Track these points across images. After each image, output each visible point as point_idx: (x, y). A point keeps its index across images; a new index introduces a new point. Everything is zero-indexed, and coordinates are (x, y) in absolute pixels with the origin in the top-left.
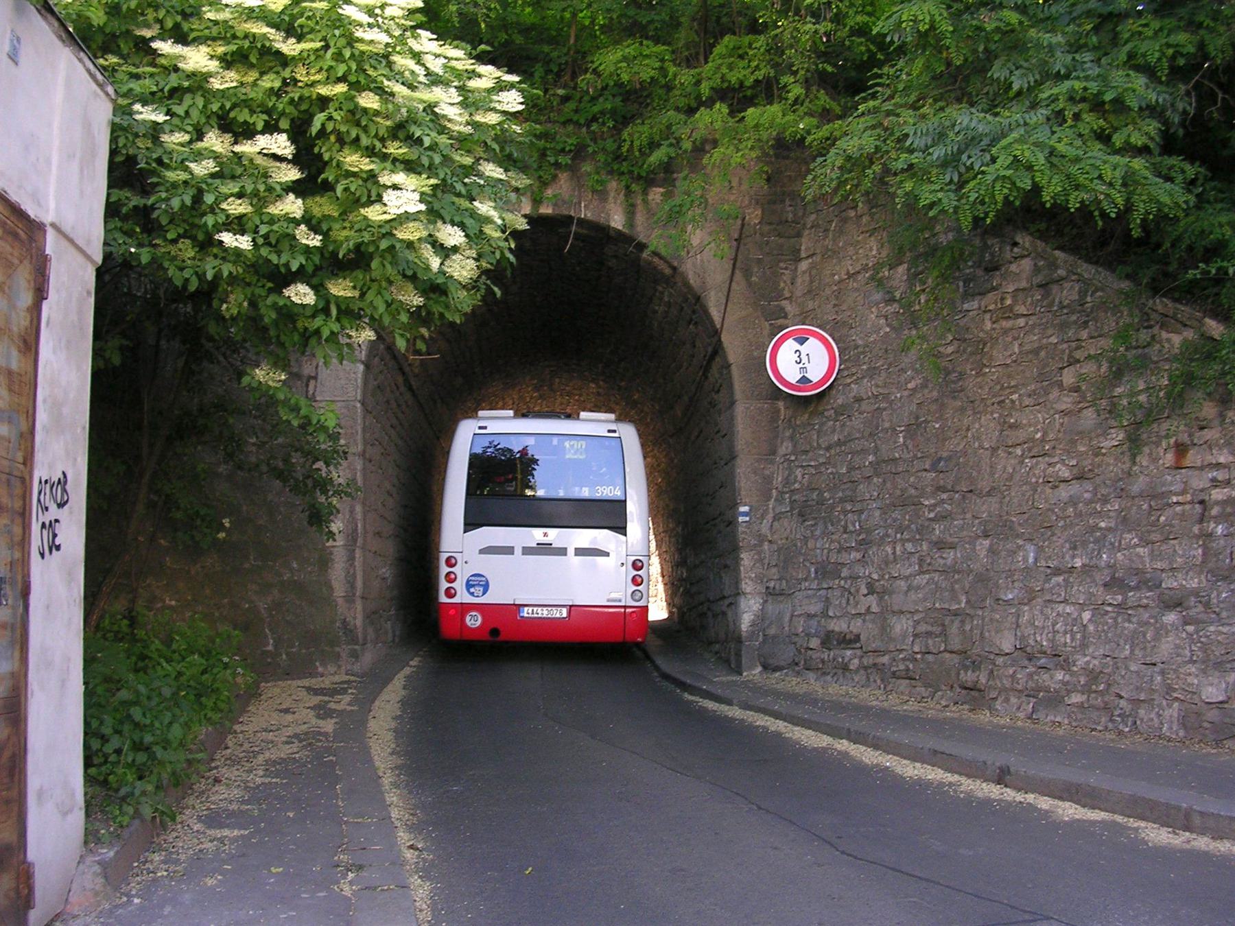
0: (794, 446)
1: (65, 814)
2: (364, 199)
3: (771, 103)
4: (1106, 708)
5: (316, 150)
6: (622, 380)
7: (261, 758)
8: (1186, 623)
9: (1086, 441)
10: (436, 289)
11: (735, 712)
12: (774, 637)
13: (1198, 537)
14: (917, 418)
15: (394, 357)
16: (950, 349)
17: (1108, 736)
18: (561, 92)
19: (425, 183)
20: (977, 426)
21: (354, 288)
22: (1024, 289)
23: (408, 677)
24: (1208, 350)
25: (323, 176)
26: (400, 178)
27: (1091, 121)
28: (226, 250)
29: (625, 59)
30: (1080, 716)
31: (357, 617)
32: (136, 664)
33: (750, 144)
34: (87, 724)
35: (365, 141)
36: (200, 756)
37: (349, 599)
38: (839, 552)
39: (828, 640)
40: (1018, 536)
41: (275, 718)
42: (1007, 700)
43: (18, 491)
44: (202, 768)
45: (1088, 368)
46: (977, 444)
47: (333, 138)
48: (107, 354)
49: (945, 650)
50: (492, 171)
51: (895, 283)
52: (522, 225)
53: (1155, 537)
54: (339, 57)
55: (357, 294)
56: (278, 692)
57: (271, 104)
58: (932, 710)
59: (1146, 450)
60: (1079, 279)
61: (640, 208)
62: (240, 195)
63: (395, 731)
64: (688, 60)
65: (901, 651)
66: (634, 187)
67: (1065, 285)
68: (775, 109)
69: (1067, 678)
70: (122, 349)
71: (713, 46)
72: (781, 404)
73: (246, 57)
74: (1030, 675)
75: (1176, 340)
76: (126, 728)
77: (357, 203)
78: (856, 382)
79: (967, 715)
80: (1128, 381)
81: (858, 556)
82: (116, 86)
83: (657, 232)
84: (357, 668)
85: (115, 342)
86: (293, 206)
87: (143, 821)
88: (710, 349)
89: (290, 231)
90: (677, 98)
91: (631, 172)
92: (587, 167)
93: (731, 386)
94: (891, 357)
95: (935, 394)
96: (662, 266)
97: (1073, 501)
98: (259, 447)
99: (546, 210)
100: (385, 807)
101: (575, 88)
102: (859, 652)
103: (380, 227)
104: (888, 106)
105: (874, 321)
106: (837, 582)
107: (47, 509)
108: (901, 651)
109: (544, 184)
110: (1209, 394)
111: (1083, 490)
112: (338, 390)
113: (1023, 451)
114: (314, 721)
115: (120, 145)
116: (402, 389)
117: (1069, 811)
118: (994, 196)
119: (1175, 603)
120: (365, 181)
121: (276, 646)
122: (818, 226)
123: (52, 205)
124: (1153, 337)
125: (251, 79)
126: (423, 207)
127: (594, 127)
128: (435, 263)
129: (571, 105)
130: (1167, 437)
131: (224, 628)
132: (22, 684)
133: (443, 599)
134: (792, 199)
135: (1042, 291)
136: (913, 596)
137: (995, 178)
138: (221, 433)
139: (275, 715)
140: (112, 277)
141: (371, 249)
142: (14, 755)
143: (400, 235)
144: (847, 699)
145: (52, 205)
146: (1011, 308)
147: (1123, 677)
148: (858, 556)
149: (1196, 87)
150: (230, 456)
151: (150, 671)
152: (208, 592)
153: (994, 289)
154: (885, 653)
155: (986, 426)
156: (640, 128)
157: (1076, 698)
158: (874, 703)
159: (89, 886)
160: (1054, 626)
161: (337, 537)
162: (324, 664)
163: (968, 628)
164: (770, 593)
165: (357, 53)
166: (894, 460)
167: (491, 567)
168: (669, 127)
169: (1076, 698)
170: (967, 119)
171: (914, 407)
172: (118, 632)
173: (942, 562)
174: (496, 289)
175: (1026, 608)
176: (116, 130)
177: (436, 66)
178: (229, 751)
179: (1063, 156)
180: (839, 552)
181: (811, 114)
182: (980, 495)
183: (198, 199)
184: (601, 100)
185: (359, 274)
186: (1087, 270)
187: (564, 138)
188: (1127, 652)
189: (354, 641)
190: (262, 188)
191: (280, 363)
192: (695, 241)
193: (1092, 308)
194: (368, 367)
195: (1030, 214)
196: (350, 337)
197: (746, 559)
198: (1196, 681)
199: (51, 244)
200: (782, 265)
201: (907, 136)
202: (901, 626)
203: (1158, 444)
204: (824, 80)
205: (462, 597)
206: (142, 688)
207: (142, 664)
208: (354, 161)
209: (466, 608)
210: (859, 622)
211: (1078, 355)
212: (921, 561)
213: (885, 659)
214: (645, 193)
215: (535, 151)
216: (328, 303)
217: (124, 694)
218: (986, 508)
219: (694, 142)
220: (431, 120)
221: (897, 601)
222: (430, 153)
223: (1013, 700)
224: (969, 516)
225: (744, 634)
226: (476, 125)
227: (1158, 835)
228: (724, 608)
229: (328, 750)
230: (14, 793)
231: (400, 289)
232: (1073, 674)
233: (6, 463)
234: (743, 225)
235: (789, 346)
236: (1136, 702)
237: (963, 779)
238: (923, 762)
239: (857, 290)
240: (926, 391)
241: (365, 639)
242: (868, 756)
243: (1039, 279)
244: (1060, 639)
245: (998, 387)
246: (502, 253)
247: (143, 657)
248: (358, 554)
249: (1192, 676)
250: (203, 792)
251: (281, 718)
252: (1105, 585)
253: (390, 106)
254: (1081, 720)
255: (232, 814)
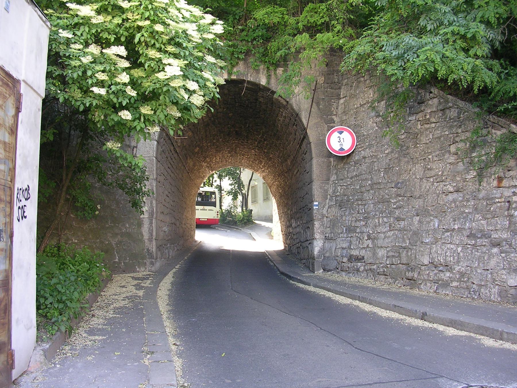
0: (337, 177)
1: (28, 329)
2: (157, 70)
3: (328, 32)
4: (467, 288)
5: (136, 49)
6: (265, 149)
7: (112, 306)
8: (501, 253)
9: (460, 176)
10: (186, 108)
11: (311, 289)
12: (328, 257)
13: (507, 216)
14: (389, 165)
15: (170, 139)
16: (403, 137)
17: (468, 300)
18: (240, 27)
19: (182, 63)
20: (414, 169)
21: (152, 110)
22: (435, 112)
23: (174, 273)
24: (513, 137)
25: (139, 60)
26: (171, 61)
27: (460, 43)
28: (95, 94)
29: (267, 13)
30: (456, 291)
31: (153, 247)
32: (60, 266)
33: (318, 49)
34: (38, 291)
35: (157, 45)
36: (86, 305)
37: (150, 240)
38: (355, 222)
39: (351, 258)
40: (431, 215)
41: (118, 290)
42: (426, 284)
43: (8, 193)
44: (87, 310)
45: (461, 145)
46: (414, 177)
47: (143, 44)
48: (47, 136)
49: (400, 263)
50: (210, 59)
51: (381, 109)
52: (223, 82)
53: (488, 216)
54: (146, 8)
55: (153, 112)
56: (119, 279)
57: (117, 31)
58: (394, 288)
59: (485, 180)
60: (458, 107)
61: (273, 76)
62: (103, 71)
63: (169, 295)
64: (293, 14)
65: (381, 263)
66: (271, 68)
67: (452, 110)
68: (330, 34)
69: (451, 275)
70: (54, 134)
71: (304, 8)
72: (332, 159)
73: (106, 10)
74: (436, 274)
75: (498, 133)
76: (55, 294)
77: (154, 71)
78: (363, 150)
79: (409, 290)
80: (478, 151)
81: (364, 223)
82: (51, 23)
83: (280, 87)
84: (153, 269)
85: (50, 132)
86: (124, 78)
87: (61, 332)
88: (302, 137)
89: (123, 89)
90: (289, 30)
91: (269, 61)
92: (251, 60)
93: (311, 152)
94: (378, 140)
95: (397, 155)
96: (282, 101)
97: (454, 201)
98: (112, 175)
99: (234, 77)
100: (164, 327)
101: (246, 26)
102: (364, 264)
103: (163, 81)
104: (376, 34)
105: (371, 125)
106: (355, 234)
107: (21, 201)
108: (381, 263)
109: (233, 66)
110: (512, 157)
111: (458, 196)
112: (146, 151)
113: (433, 179)
114: (135, 291)
115: (53, 47)
116: (173, 152)
117: (451, 331)
118: (418, 73)
119: (497, 244)
120: (157, 62)
121: (119, 260)
122: (348, 84)
123: (23, 72)
124: (489, 132)
125: (108, 20)
126: (182, 73)
127: (255, 42)
128: (186, 96)
129: (245, 33)
130: (494, 174)
131: (97, 252)
132: (10, 274)
134: (337, 73)
135: (442, 112)
136: (387, 240)
137: (417, 65)
138: (96, 169)
139: (118, 288)
140: (49, 103)
141: (160, 91)
142: (6, 304)
143: (172, 84)
144: (358, 284)
145: (23, 72)
146: (429, 119)
147: (474, 275)
148: (364, 223)
149: (507, 27)
150: (100, 179)
151: (66, 270)
152: (91, 236)
153: (422, 111)
154: (374, 264)
155: (418, 169)
156: (273, 43)
157: (455, 284)
158: (370, 285)
159: (38, 359)
160: (446, 253)
161: (145, 213)
162: (139, 267)
163: (409, 254)
164: (326, 239)
165: (154, 7)
166: (379, 183)
168: (285, 42)
169: (455, 284)
170: (409, 39)
171: (388, 161)
172: (53, 253)
173: (399, 226)
174: (211, 109)
175: (434, 246)
176: (51, 41)
177: (187, 15)
178: (99, 303)
179: (448, 57)
180: (355, 222)
181: (344, 37)
182: (415, 198)
183: (84, 72)
184: (257, 31)
185: (153, 102)
186: (461, 104)
187: (241, 47)
188: (476, 265)
189: (152, 257)
190: (113, 69)
191: (121, 140)
192: (296, 91)
193: (463, 120)
194: (158, 142)
195: (432, 80)
196: (149, 130)
197: (317, 224)
198: (505, 277)
199: (23, 89)
200: (332, 101)
201: (383, 46)
202: (381, 253)
203: (490, 177)
204: (351, 23)
206: (61, 277)
207: (62, 266)
208: (153, 53)
210: (364, 251)
211: (457, 139)
212: (390, 226)
213: (375, 267)
214: (275, 70)
215: (230, 50)
216: (140, 115)
217: (54, 281)
218: (418, 203)
219: (296, 49)
220: (185, 37)
221: (380, 242)
222: (184, 51)
223: (428, 284)
224: (410, 207)
225: (316, 256)
226: (204, 39)
227: (489, 342)
228: (307, 245)
229: (140, 303)
230: (7, 320)
231: (171, 109)
232: (453, 274)
233: (3, 181)
234: (316, 84)
235: (336, 135)
236: (480, 286)
237: (407, 318)
238: (390, 310)
239: (364, 111)
240: (393, 154)
241: (157, 257)
242: (367, 307)
243: (441, 107)
244: (448, 259)
245: (423, 153)
246: (214, 94)
247: (63, 264)
248: (154, 221)
249: (504, 275)
250: (87, 320)
251: (121, 290)
252: (468, 236)
253: (168, 30)
254: (457, 293)
255: (99, 330)
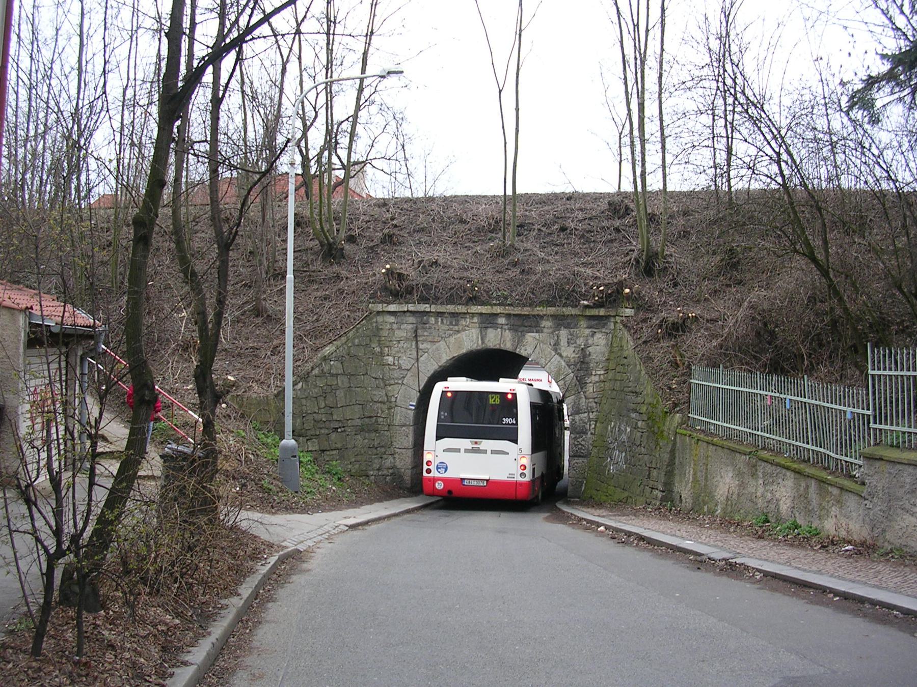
133: (425, 474)
167: (447, 458)
205: (434, 474)
209: (435, 480)
